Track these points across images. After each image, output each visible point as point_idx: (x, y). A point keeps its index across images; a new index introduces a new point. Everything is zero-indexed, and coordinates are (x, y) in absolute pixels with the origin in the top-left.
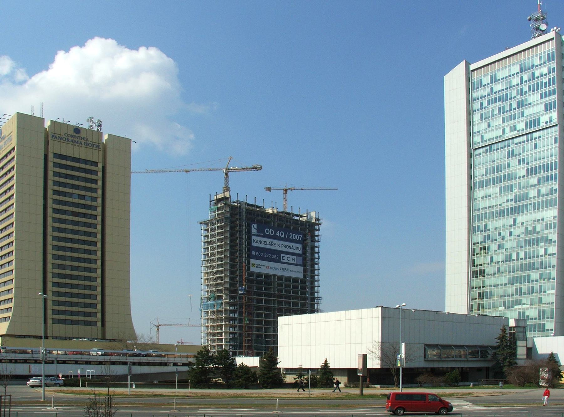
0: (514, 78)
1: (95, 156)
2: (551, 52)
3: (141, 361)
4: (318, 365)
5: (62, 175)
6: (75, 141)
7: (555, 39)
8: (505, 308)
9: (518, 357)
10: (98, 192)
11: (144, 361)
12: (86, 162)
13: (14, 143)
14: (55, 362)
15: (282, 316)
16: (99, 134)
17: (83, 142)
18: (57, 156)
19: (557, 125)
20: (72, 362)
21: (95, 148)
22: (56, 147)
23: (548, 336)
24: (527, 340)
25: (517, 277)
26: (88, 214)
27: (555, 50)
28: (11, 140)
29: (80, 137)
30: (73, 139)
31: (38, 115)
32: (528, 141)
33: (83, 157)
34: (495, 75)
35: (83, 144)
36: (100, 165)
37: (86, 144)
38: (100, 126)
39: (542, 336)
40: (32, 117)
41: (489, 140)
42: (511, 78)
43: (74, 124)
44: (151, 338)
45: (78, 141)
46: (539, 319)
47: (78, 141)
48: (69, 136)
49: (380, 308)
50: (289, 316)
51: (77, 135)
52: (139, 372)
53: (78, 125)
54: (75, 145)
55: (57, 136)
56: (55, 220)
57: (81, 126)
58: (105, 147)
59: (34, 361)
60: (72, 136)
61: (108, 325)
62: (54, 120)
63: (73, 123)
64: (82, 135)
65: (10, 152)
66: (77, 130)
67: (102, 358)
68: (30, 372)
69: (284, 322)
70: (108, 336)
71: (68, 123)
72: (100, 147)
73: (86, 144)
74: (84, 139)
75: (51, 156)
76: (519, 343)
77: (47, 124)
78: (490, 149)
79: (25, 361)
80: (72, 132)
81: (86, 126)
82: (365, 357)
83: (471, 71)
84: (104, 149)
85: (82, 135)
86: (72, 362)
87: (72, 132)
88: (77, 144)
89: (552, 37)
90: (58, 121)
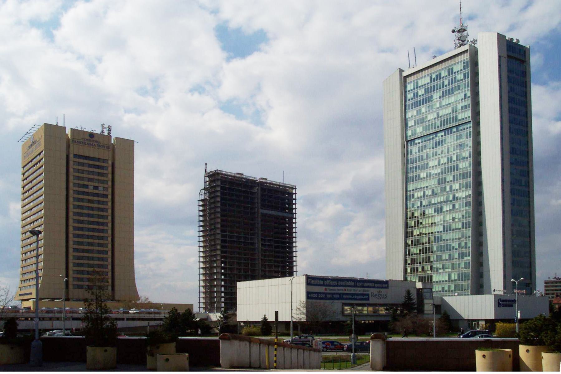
0: (458, 74)
1: (105, 154)
2: (466, 61)
3: (134, 317)
4: (260, 319)
5: (80, 171)
6: (90, 144)
7: (469, 50)
8: (432, 272)
9: (425, 312)
10: (109, 184)
11: (136, 317)
12: (98, 160)
13: (42, 147)
14: (71, 319)
15: (239, 281)
16: (109, 136)
17: (96, 144)
18: (76, 156)
19: (471, 121)
20: (47, 319)
21: (106, 149)
22: (75, 149)
23: (452, 296)
24: (433, 299)
25: (426, 248)
26: (101, 201)
27: (469, 60)
28: (40, 145)
29: (94, 140)
30: (88, 142)
31: (61, 124)
32: (422, 142)
33: (97, 156)
34: (452, 69)
35: (97, 146)
36: (110, 162)
37: (99, 146)
38: (110, 130)
39: (464, 295)
40: (57, 127)
41: (463, 119)
42: (456, 75)
43: (89, 131)
44: (147, 299)
45: (92, 144)
46: (459, 280)
47: (92, 144)
48: (85, 140)
49: (305, 276)
50: (244, 282)
51: (92, 139)
52: (133, 326)
53: (92, 132)
54: (90, 147)
55: (76, 140)
56: (75, 207)
57: (94, 132)
58: (113, 145)
59: (56, 319)
60: (87, 140)
61: (116, 288)
62: (74, 128)
63: (88, 130)
64: (96, 139)
65: (40, 154)
66: (92, 135)
67: (137, 316)
68: (52, 327)
69: (240, 285)
70: (117, 298)
71: (85, 130)
72: (110, 148)
73: (99, 146)
74: (97, 142)
75: (71, 156)
76: (426, 301)
77: (68, 132)
78: (457, 130)
79: (51, 319)
80: (87, 137)
81: (98, 131)
82: (277, 313)
83: (404, 77)
84: (112, 149)
85: (96, 139)
86: (47, 319)
87: (87, 137)
88: (91, 146)
89: (466, 49)
90: (77, 128)
